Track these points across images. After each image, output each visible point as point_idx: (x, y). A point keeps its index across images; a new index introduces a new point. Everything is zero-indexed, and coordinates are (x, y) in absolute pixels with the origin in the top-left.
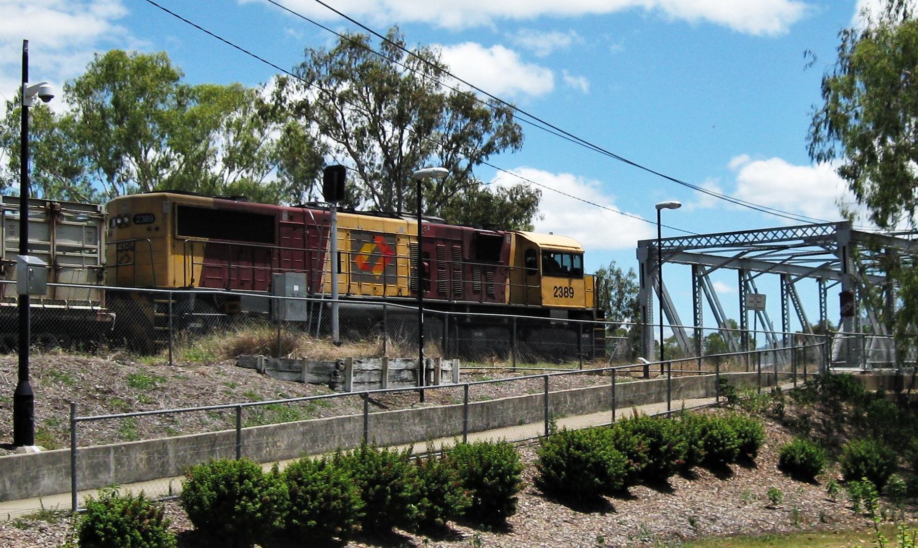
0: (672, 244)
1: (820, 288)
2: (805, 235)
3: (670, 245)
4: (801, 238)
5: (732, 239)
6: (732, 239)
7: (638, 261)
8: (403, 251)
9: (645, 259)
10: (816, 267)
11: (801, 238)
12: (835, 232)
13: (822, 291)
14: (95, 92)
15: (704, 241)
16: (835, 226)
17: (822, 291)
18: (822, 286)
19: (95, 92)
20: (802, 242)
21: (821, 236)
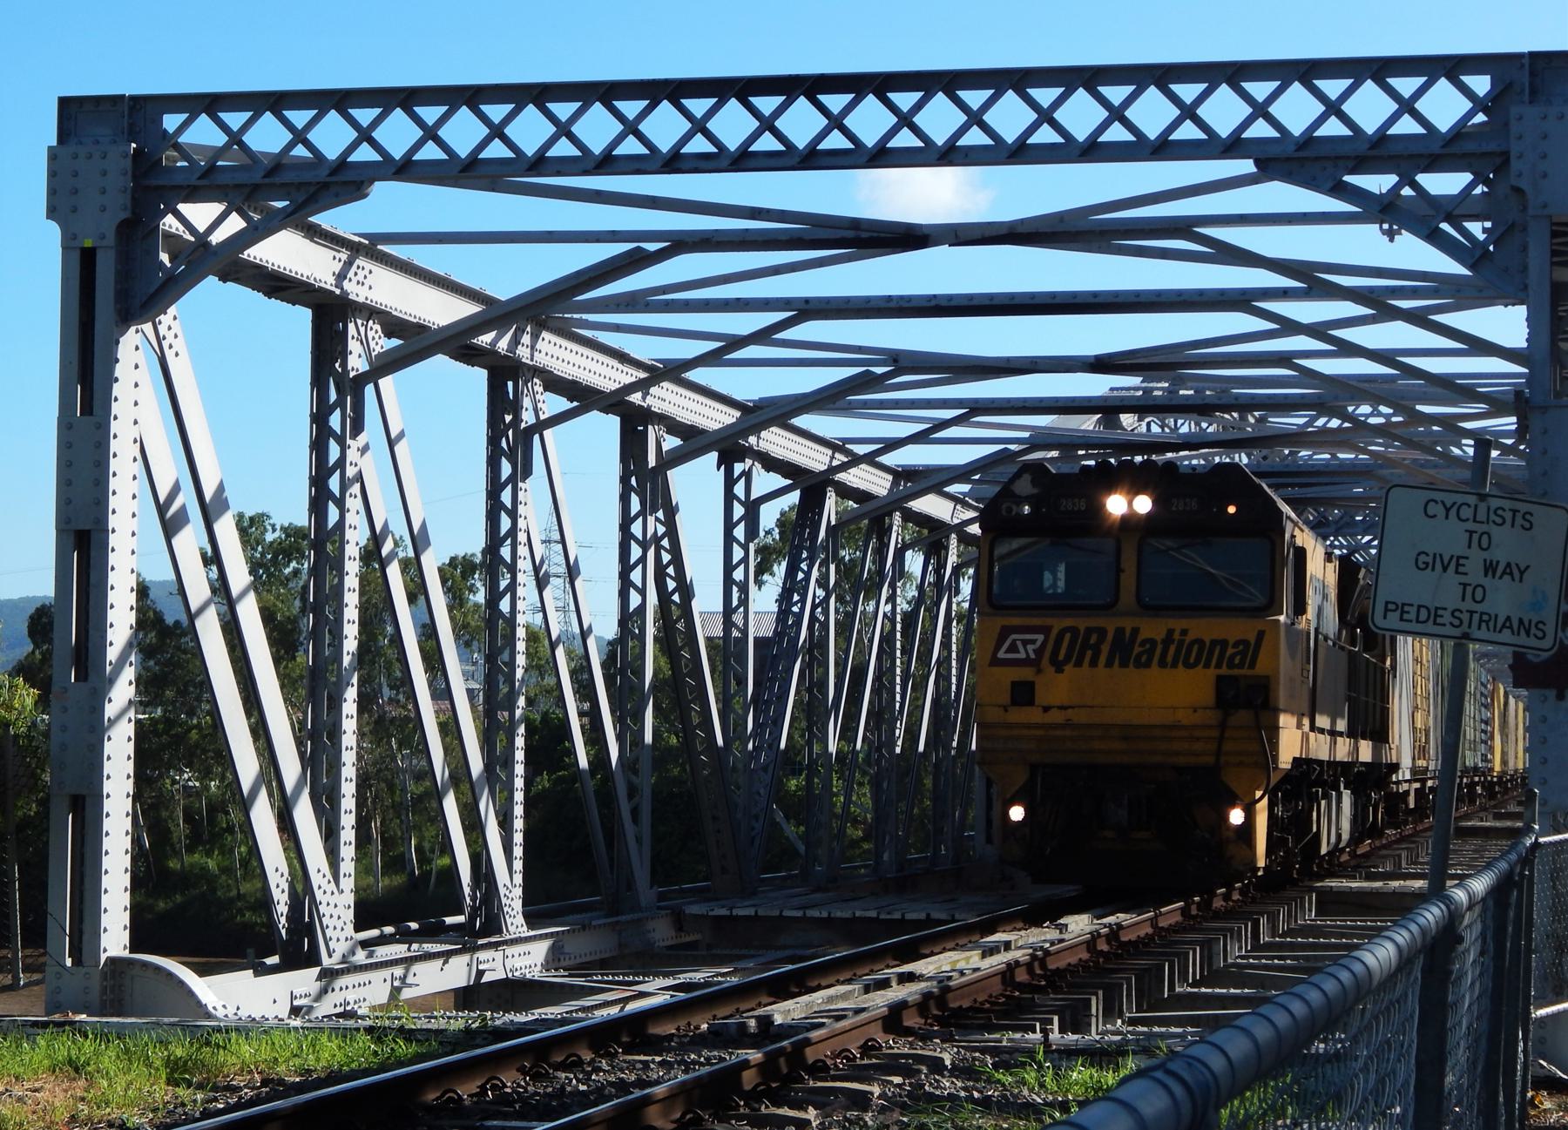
0: (235, 138)
1: (729, 497)
2: (1261, 129)
3: (220, 139)
4: (1233, 146)
5: (463, 132)
6: (463, 132)
7: (54, 231)
8: (1247, 665)
9: (109, 226)
10: (752, 348)
11: (1233, 146)
12: (1481, 118)
13: (738, 511)
14: (162, 1092)
15: (801, 123)
16: (1481, 84)
17: (738, 511)
18: (739, 489)
19: (162, 1092)
20: (1247, 166)
21: (1382, 137)
